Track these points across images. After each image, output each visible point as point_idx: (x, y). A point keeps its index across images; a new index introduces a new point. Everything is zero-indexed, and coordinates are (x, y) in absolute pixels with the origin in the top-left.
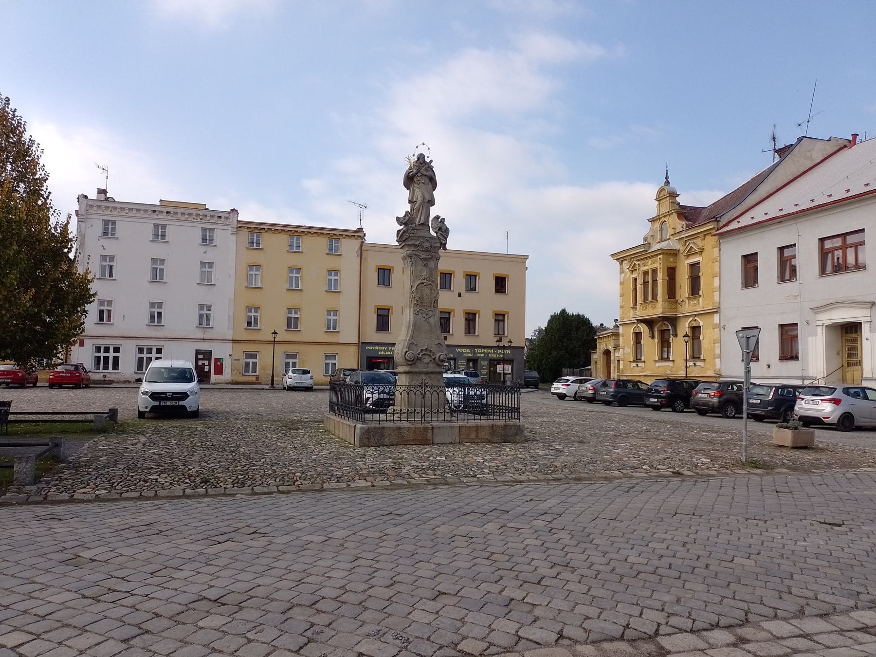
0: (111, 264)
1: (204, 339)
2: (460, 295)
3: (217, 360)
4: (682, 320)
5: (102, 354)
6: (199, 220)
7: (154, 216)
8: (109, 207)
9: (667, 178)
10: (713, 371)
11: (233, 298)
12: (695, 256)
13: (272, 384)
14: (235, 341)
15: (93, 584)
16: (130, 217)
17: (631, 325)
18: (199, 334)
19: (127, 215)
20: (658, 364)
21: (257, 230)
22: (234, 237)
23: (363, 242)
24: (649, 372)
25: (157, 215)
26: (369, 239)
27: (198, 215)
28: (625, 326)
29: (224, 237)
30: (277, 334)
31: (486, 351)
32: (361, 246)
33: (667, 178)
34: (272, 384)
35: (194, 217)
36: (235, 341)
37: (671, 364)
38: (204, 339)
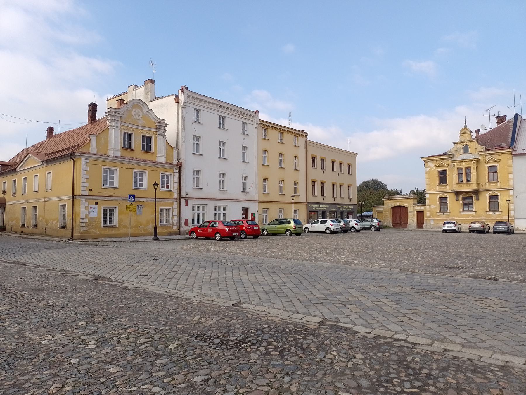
0: (197, 142)
1: (245, 200)
2: (338, 174)
3: (252, 215)
4: (482, 192)
5: (217, 212)
6: (241, 116)
7: (220, 109)
8: (198, 99)
9: (465, 123)
10: (213, 219)
11: (257, 172)
12: (496, 162)
13: (156, 234)
14: (260, 202)
15: (501, 324)
16: (208, 108)
17: (437, 194)
18: (243, 197)
19: (207, 106)
20: (462, 214)
21: (266, 126)
22: (256, 130)
23: (307, 140)
24: (454, 217)
25: (222, 109)
26: (309, 138)
27: (241, 112)
28: (430, 194)
29: (252, 129)
30: (509, 201)
31: (318, 206)
32: (306, 142)
33: (465, 123)
34: (156, 234)
35: (239, 113)
36: (260, 202)
37: (474, 213)
38: (245, 200)
